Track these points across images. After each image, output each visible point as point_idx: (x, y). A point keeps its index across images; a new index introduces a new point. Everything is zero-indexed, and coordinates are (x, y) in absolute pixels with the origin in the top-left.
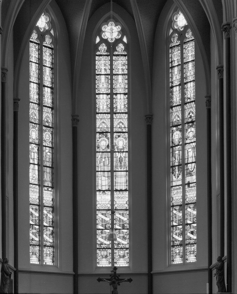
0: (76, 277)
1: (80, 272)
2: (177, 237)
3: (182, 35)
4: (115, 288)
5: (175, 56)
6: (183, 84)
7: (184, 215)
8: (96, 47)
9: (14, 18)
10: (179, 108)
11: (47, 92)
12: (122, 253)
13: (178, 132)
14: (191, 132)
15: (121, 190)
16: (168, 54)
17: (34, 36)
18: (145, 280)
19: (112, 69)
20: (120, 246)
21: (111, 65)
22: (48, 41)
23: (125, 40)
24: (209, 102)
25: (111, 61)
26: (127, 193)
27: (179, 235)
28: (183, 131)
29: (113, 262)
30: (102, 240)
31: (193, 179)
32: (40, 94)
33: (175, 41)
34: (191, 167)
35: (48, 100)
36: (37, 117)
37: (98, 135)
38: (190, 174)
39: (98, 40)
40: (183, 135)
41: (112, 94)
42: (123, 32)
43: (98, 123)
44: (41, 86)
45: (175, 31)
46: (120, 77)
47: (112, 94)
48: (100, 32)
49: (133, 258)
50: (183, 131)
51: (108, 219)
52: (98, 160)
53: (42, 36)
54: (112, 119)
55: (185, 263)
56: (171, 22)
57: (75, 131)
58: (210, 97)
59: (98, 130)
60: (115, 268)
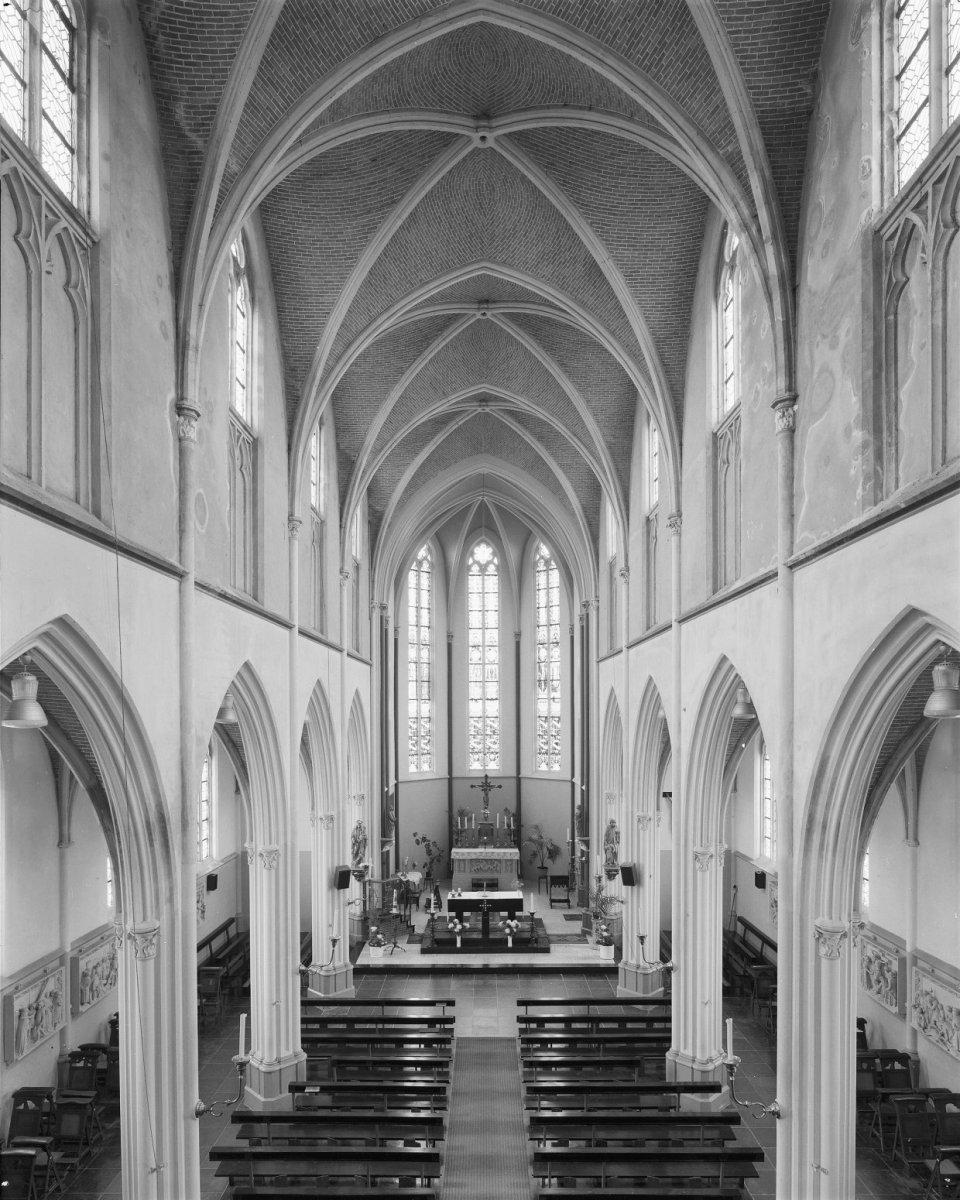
0: (450, 780)
1: (455, 775)
4: (487, 795)
5: (542, 579)
6: (548, 607)
8: (469, 568)
11: (424, 613)
12: (492, 756)
13: (544, 650)
14: (556, 652)
15: (492, 699)
16: (534, 576)
18: (514, 782)
19: (483, 588)
20: (492, 750)
22: (425, 566)
23: (496, 561)
25: (483, 580)
29: (485, 765)
30: (475, 745)
31: (557, 695)
32: (418, 617)
33: (541, 566)
36: (415, 638)
37: (470, 649)
39: (471, 561)
41: (484, 611)
42: (494, 554)
43: (471, 637)
44: (418, 608)
47: (484, 611)
48: (472, 554)
51: (480, 725)
52: (471, 671)
54: (484, 633)
55: (549, 772)
57: (449, 646)
59: (471, 644)
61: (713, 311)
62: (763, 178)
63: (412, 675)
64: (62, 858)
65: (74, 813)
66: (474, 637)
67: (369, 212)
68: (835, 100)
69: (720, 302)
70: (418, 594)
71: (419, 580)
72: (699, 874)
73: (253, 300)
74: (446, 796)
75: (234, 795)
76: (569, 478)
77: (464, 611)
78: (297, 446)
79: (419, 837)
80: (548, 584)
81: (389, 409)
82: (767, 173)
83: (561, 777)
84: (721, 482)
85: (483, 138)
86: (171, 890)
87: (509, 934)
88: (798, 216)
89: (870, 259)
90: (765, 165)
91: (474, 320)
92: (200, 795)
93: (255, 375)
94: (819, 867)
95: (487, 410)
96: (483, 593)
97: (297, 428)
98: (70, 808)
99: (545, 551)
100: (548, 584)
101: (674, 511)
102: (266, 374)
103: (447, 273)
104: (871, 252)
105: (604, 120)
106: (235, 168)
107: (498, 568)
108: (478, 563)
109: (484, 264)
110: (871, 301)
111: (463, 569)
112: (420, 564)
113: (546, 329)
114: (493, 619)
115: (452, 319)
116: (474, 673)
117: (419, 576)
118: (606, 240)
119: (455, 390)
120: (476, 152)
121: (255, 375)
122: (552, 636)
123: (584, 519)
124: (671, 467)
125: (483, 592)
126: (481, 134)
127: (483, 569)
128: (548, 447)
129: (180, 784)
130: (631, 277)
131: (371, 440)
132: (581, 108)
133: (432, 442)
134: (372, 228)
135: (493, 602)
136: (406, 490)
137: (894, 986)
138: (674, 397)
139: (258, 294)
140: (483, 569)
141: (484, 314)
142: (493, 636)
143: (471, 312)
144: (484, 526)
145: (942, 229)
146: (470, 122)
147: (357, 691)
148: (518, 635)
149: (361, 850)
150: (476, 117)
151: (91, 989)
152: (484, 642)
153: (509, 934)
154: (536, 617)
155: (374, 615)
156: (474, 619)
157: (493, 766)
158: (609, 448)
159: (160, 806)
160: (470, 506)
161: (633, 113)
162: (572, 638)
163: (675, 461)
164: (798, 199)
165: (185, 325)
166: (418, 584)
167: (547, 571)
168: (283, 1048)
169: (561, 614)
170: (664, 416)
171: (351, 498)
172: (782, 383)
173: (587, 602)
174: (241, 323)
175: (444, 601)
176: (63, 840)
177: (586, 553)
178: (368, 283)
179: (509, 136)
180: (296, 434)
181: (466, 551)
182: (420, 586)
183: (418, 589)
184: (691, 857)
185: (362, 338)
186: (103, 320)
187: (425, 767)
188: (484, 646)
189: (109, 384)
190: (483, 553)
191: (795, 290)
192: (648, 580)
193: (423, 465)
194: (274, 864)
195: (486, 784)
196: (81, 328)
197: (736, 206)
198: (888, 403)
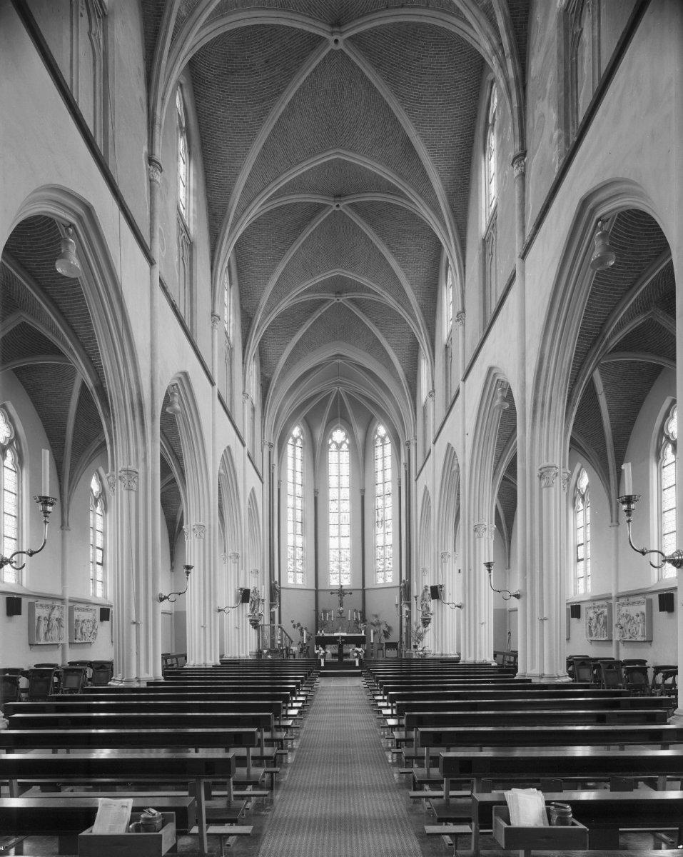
0: (317, 591)
2: (380, 566)
3: (383, 440)
5: (379, 452)
6: (384, 470)
7: (384, 552)
8: (329, 446)
9: (30, 321)
10: (381, 485)
12: (346, 576)
14: (389, 501)
15: (345, 537)
16: (374, 450)
17: (290, 441)
19: (339, 461)
21: (339, 457)
22: (299, 443)
23: (347, 441)
24: (400, 482)
26: (349, 539)
27: (381, 565)
28: (384, 499)
31: (390, 530)
32: (294, 477)
33: (379, 443)
34: (389, 522)
35: (299, 480)
38: (388, 526)
39: (330, 441)
40: (384, 502)
41: (339, 476)
42: (346, 436)
44: (294, 471)
45: (379, 436)
46: (344, 465)
47: (339, 476)
48: (331, 436)
49: (353, 580)
50: (384, 499)
51: (337, 555)
53: (295, 441)
56: (376, 431)
57: (316, 499)
58: (400, 479)
59: (331, 499)
60: (342, 586)
61: (483, 162)
62: (504, 14)
63: (290, 516)
64: (63, 537)
65: (71, 507)
66: (333, 494)
67: (264, 100)
68: (653, 587)
69: (487, 154)
70: (294, 461)
71: (294, 451)
72: (477, 540)
73: (190, 153)
74: (314, 601)
75: (169, 571)
76: (397, 355)
77: (326, 476)
78: (217, 266)
79: (296, 623)
80: (384, 455)
81: (276, 279)
82: (507, 12)
83: (395, 585)
84: (488, 270)
85: (336, 41)
86: (145, 454)
87: (356, 657)
88: (526, 41)
89: (562, 27)
90: (505, 6)
93: (191, 202)
94: (541, 433)
95: (341, 300)
96: (339, 487)
97: (217, 255)
98: (68, 505)
99: (382, 430)
100: (384, 455)
101: (460, 310)
102: (197, 202)
103: (314, 156)
104: (562, 23)
105: (412, 12)
106: (184, 13)
107: (349, 446)
108: (335, 443)
109: (337, 150)
110: (562, 54)
111: (325, 447)
112: (295, 441)
114: (346, 481)
116: (333, 518)
117: (294, 449)
118: (415, 122)
119: (319, 273)
120: (332, 51)
121: (191, 202)
122: (386, 491)
123: (406, 383)
124: (458, 280)
125: (339, 463)
127: (339, 446)
128: (382, 331)
129: (150, 391)
130: (431, 148)
131: (263, 303)
132: (397, 7)
133: (304, 326)
134: (265, 113)
135: (346, 469)
136: (286, 364)
137: (605, 623)
138: (460, 234)
139: (193, 149)
140: (339, 446)
141: (338, 206)
142: (346, 493)
144: (338, 416)
146: (328, 29)
147: (253, 489)
148: (363, 491)
149: (257, 606)
150: (332, 25)
151: (81, 631)
152: (339, 497)
153: (356, 657)
154: (375, 478)
155: (265, 449)
156: (333, 481)
157: (347, 583)
158: (421, 308)
159: (139, 394)
160: (329, 395)
162: (400, 488)
163: (461, 277)
164: (526, 30)
165: (153, 109)
166: (294, 454)
167: (383, 446)
168: (208, 657)
169: (393, 475)
170: (453, 246)
171: (250, 343)
172: (517, 146)
173: (409, 441)
174: (182, 168)
175: (311, 466)
177: (405, 399)
178: (261, 156)
180: (216, 259)
181: (327, 434)
182: (295, 456)
183: (294, 458)
184: (472, 529)
185: (258, 199)
186: (110, 61)
187: (299, 581)
188: (339, 500)
189: (114, 101)
190: (339, 435)
191: (525, 88)
192: (447, 387)
193: (297, 345)
194: (202, 535)
195: (341, 592)
196: (97, 63)
197: (490, 39)
198: (572, 110)
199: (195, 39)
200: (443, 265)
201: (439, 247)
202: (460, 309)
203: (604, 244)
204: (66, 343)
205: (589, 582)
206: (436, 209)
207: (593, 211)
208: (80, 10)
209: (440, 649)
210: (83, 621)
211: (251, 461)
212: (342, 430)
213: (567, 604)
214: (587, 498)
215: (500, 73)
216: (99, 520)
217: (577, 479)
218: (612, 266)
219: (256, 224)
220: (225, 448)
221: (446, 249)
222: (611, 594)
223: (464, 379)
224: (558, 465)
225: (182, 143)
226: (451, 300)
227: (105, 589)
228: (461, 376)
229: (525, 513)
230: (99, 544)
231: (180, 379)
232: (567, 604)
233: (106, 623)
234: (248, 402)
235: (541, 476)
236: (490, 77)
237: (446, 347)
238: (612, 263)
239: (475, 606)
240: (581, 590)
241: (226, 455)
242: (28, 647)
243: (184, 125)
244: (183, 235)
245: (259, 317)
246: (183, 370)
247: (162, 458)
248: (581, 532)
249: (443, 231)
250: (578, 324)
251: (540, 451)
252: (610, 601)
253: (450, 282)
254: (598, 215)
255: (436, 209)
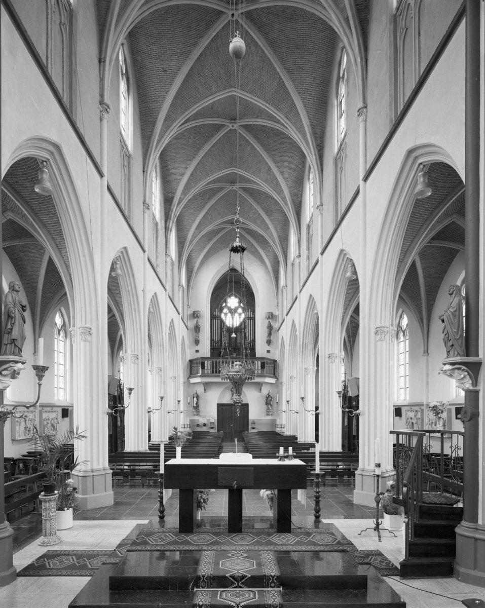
48: (225, 301)
61: (308, 184)
72: (331, 364)
85: (233, 126)
91: (229, 190)
92: (463, 314)
95: (234, 188)
113: (256, 194)
115: (224, 228)
120: (231, 190)
126: (234, 128)
143: (227, 186)
145: (402, 30)
147: (172, 320)
161: (271, 118)
163: (320, 184)
176: (427, 352)
179: (241, 125)
199: (133, 15)
200: (307, 170)
201: (303, 157)
202: (319, 203)
203: (424, 181)
204: (42, 237)
205: (408, 392)
206: (301, 129)
207: (416, 158)
208: (53, 9)
209: (303, 438)
210: (52, 419)
211: (172, 301)
212: (236, 297)
213: (394, 406)
214: (407, 333)
215: (349, 40)
216: (61, 344)
217: (400, 319)
218: (430, 195)
219: (175, 138)
220: (153, 294)
221: (308, 158)
222: (423, 403)
223: (322, 254)
224: (388, 326)
225: (123, 86)
226: (312, 205)
227: (65, 394)
228: (320, 251)
229: (364, 351)
230: (61, 385)
231: (122, 252)
232: (394, 406)
233: (67, 419)
234: (168, 260)
235: (376, 333)
236: (341, 45)
237: (309, 227)
238: (430, 194)
239: (329, 419)
240: (402, 397)
241: (154, 298)
242: (11, 442)
243: (124, 72)
244: (124, 150)
245: (176, 201)
246: (124, 246)
247: (108, 305)
248: (402, 356)
249: (308, 150)
250: (403, 233)
251: (377, 294)
252: (422, 408)
253: (311, 181)
254: (420, 161)
255: (301, 129)
